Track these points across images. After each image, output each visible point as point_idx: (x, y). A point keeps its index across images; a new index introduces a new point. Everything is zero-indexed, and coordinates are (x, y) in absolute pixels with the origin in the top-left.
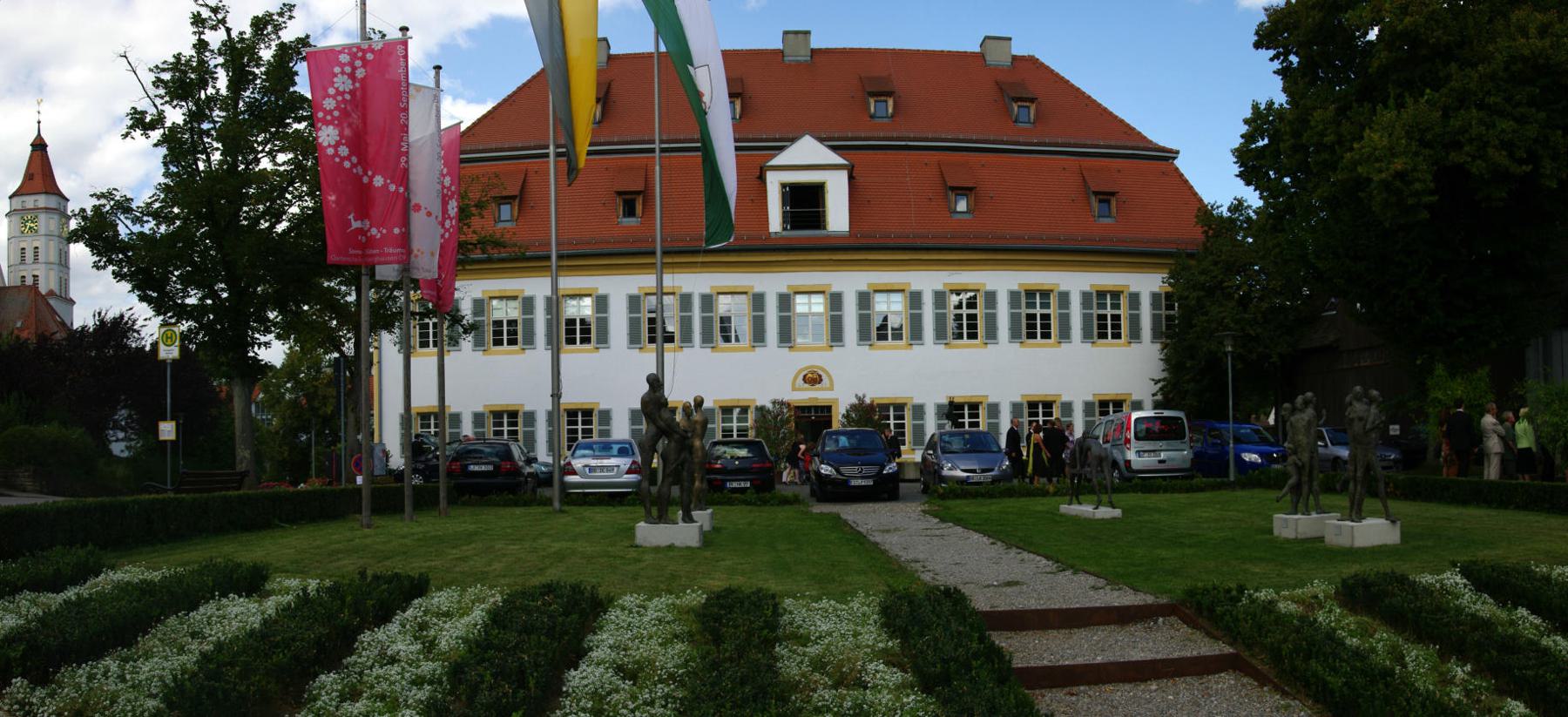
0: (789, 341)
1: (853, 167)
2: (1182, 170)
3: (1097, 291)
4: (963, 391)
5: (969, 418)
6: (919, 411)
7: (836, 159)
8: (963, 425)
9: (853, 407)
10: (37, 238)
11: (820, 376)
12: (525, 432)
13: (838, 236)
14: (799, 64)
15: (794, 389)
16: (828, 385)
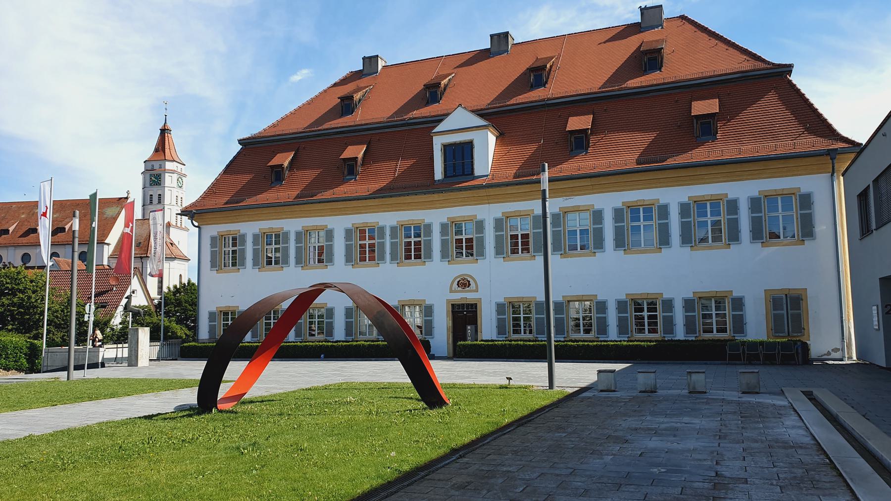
2: (794, 82)
11: (469, 282)
15: (451, 291)
16: (474, 288)
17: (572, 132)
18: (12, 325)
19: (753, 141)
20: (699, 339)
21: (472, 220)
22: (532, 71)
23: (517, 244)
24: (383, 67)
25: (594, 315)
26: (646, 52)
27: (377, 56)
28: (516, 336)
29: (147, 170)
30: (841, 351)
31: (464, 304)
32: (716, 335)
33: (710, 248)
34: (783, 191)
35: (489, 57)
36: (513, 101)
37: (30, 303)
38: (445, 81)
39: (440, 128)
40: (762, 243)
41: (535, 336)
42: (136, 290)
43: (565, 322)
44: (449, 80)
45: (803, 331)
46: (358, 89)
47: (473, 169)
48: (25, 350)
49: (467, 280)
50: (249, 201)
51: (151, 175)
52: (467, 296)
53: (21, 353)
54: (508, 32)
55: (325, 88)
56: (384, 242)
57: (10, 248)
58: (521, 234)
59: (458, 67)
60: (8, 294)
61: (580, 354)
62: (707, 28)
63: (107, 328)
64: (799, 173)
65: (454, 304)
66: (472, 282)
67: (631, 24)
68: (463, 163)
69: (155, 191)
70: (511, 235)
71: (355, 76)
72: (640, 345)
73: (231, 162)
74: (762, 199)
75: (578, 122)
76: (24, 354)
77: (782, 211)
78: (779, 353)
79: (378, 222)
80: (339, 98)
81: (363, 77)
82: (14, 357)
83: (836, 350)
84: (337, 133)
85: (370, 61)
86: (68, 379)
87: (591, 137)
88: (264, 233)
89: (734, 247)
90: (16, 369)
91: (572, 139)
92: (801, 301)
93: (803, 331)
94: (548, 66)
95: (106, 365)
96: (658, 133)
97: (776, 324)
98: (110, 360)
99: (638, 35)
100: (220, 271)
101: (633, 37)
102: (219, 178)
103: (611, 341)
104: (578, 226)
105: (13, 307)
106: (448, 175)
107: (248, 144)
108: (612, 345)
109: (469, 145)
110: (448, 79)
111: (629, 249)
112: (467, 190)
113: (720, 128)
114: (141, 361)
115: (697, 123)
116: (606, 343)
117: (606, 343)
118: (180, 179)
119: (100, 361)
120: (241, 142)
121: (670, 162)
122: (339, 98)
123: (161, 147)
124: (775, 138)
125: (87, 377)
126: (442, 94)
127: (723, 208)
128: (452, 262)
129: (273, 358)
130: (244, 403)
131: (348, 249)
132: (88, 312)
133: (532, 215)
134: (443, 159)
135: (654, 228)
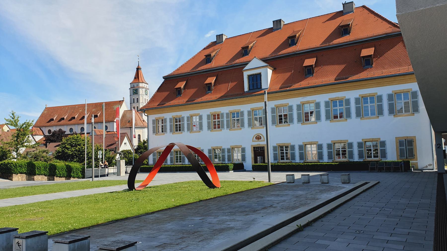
10: (138, 95)
11: (261, 137)
12: (349, 151)
15: (253, 141)
16: (263, 140)
17: (306, 67)
18: (76, 159)
19: (389, 67)
20: (365, 160)
21: (287, 106)
22: (290, 38)
23: (282, 119)
24: (226, 39)
25: (347, 150)
26: (342, 26)
27: (223, 34)
28: (282, 161)
29: (131, 87)
30: (432, 165)
31: (259, 147)
32: (373, 159)
33: (370, 118)
34: (404, 91)
35: (272, 32)
36: (281, 53)
37: (83, 150)
38: (252, 45)
39: (247, 67)
40: (330, 120)
41: (291, 161)
42: (126, 143)
43: (278, 155)
44: (254, 44)
45: (414, 156)
46: (213, 52)
47: (261, 86)
49: (260, 136)
50: (167, 104)
51: (133, 90)
52: (262, 143)
53: (79, 171)
54: (281, 19)
55: (200, 51)
56: (223, 120)
57: (76, 125)
58: (284, 115)
59: (258, 37)
60: (74, 146)
61: (305, 169)
62: (374, 12)
63: (114, 160)
64: (411, 81)
65: (254, 147)
67: (339, 11)
68: (257, 83)
69: (135, 97)
70: (279, 115)
71: (214, 44)
72: (332, 164)
73: (160, 87)
74: (394, 95)
75: (310, 62)
76: (80, 171)
77: (404, 100)
78: (377, 167)
79: (221, 111)
80: (205, 56)
81: (217, 44)
82: (76, 173)
83: (430, 165)
84: (204, 72)
85: (220, 37)
86: (92, 180)
87: (315, 68)
88: (174, 118)
89: (381, 118)
90: (77, 178)
91: (306, 70)
92: (413, 142)
93: (414, 156)
94: (297, 35)
95: (108, 175)
96: (346, 65)
97: (401, 153)
98: (111, 173)
99: (342, 17)
100: (174, 133)
101: (339, 18)
102: (155, 94)
103: (325, 162)
104: (309, 110)
105: (76, 152)
106: (250, 89)
107: (166, 78)
108: (319, 164)
109: (260, 74)
110: (253, 43)
111: (363, 117)
112: (258, 96)
113: (374, 62)
114: (122, 173)
115: (363, 60)
116: (316, 164)
117: (316, 164)
118: (146, 91)
119: (106, 174)
120: (164, 78)
121: (350, 79)
122: (205, 56)
123: (137, 76)
124: (400, 65)
125: (100, 180)
126: (250, 51)
127: (410, 96)
128: (277, 126)
129: (159, 172)
130: (147, 188)
131: (209, 123)
132: (99, 154)
133: (288, 106)
134: (248, 82)
135: (375, 107)
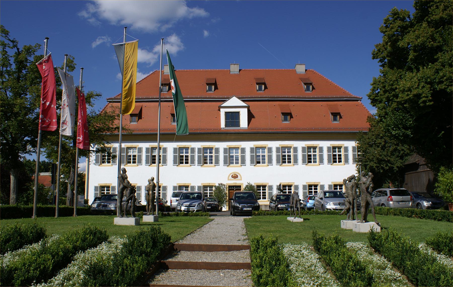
0: (271, 163)
1: (249, 107)
3: (308, 147)
4: (313, 181)
5: (314, 190)
6: (271, 188)
7: (243, 104)
8: (286, 192)
9: (247, 186)
11: (237, 176)
13: (244, 129)
14: (235, 74)
16: (240, 179)
48: (275, 192)
66: (239, 176)
